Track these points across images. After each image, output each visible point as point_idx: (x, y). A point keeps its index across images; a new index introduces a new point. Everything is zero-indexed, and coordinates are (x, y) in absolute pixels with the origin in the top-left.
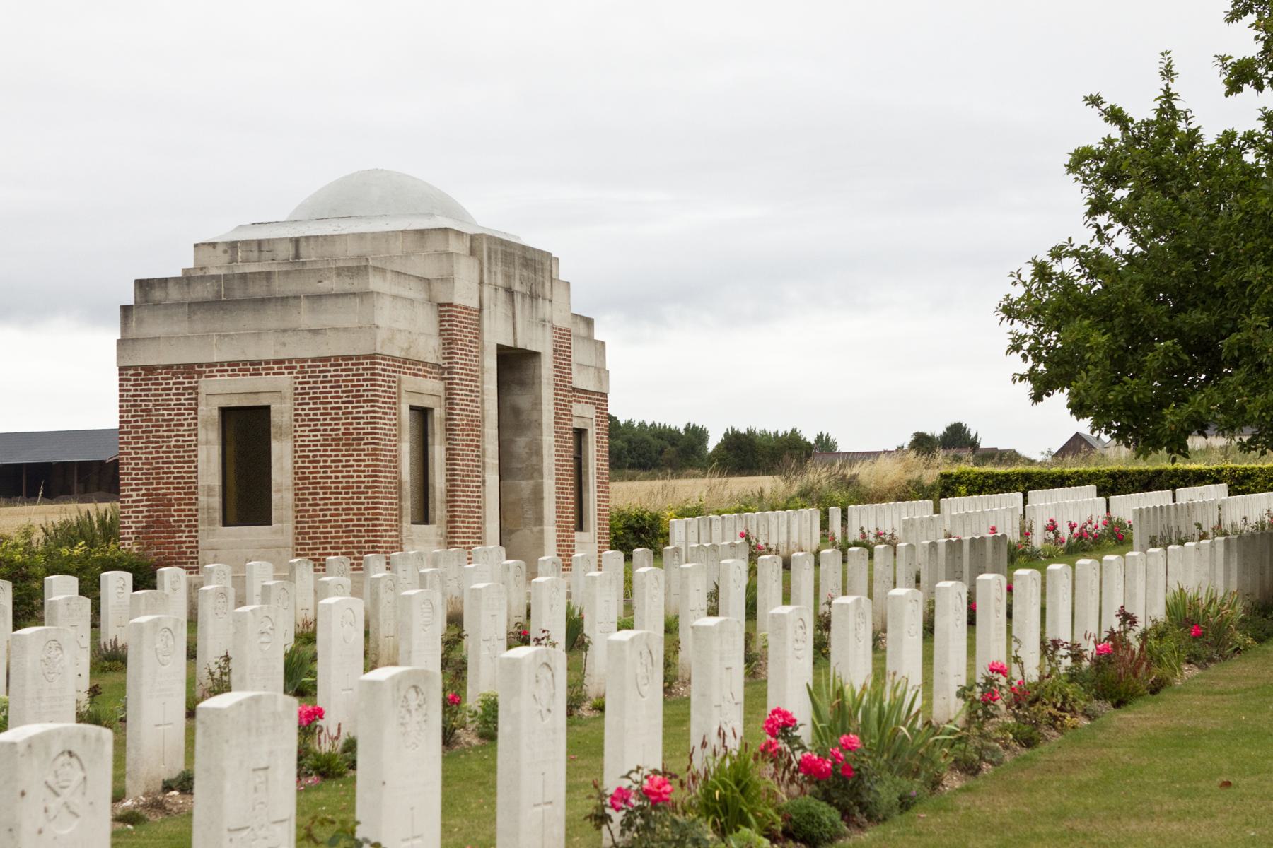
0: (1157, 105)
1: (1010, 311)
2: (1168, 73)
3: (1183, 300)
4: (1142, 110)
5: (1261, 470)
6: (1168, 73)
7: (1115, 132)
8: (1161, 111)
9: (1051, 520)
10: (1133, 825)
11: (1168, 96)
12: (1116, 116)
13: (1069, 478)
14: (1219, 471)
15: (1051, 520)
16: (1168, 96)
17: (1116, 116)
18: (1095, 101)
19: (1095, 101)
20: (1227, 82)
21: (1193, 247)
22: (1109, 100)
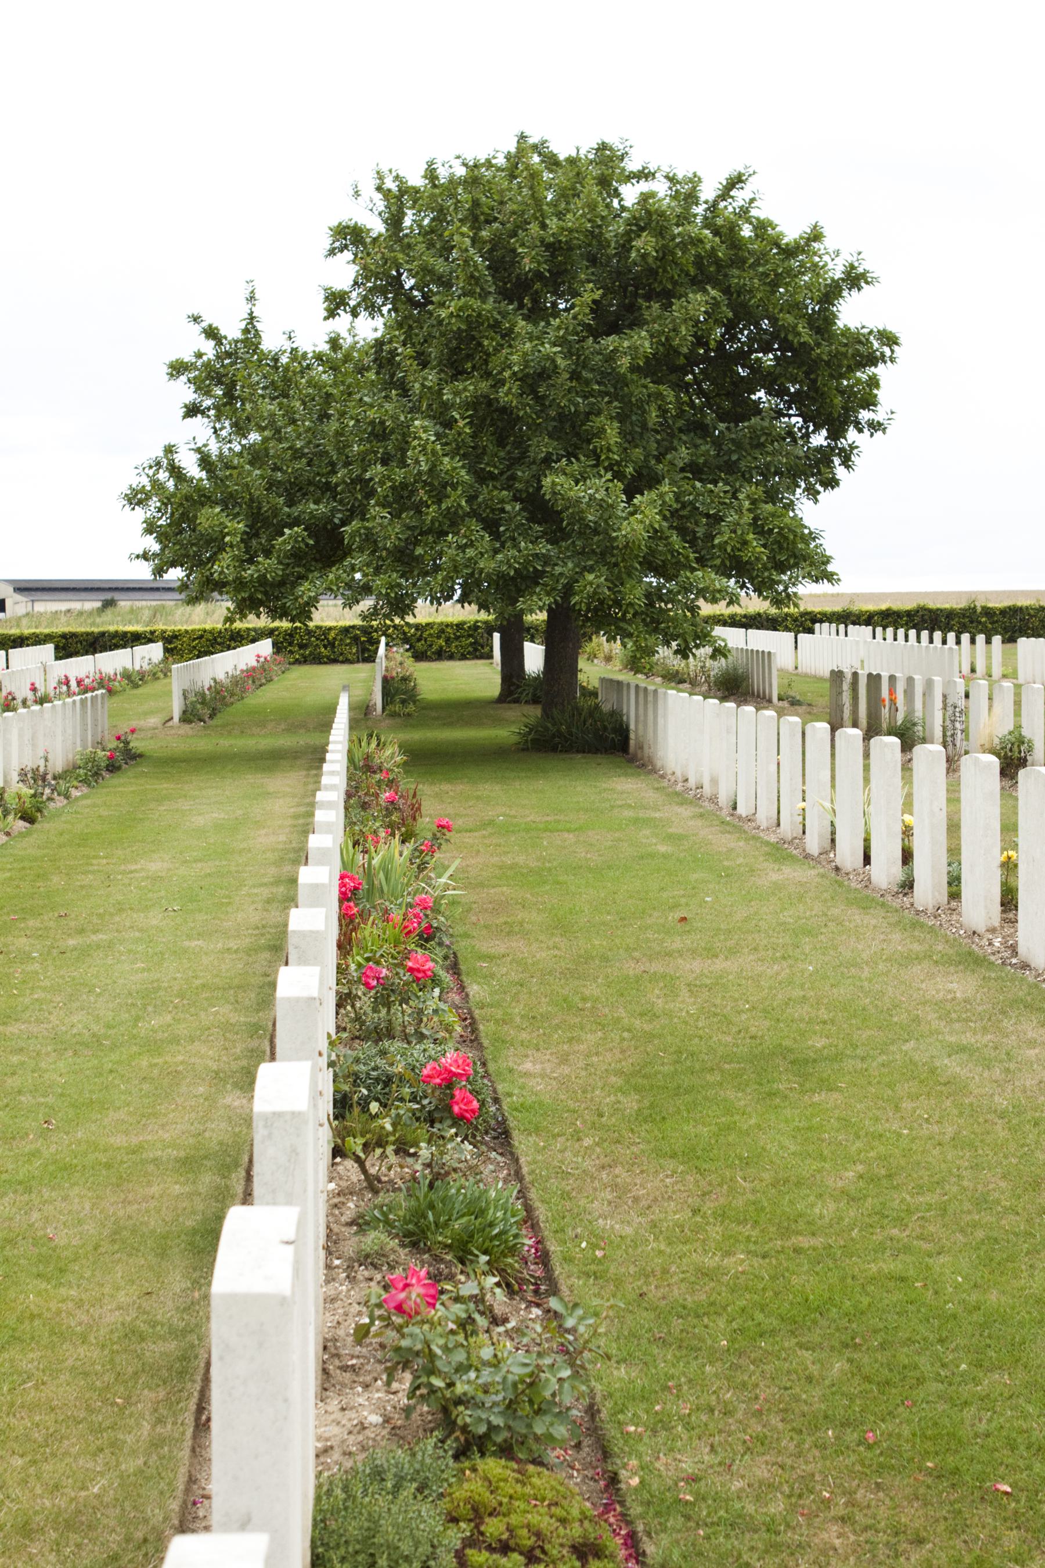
0: (243, 325)
1: (135, 498)
2: (252, 298)
3: (295, 491)
4: (232, 330)
5: (187, 632)
6: (252, 298)
7: (209, 348)
8: (246, 331)
9: (66, 676)
10: (94, 937)
11: (252, 318)
12: (211, 333)
13: (27, 638)
14: (152, 633)
15: (66, 676)
16: (252, 318)
17: (211, 333)
18: (196, 319)
19: (196, 319)
20: (327, 310)
21: (302, 447)
22: (208, 320)
